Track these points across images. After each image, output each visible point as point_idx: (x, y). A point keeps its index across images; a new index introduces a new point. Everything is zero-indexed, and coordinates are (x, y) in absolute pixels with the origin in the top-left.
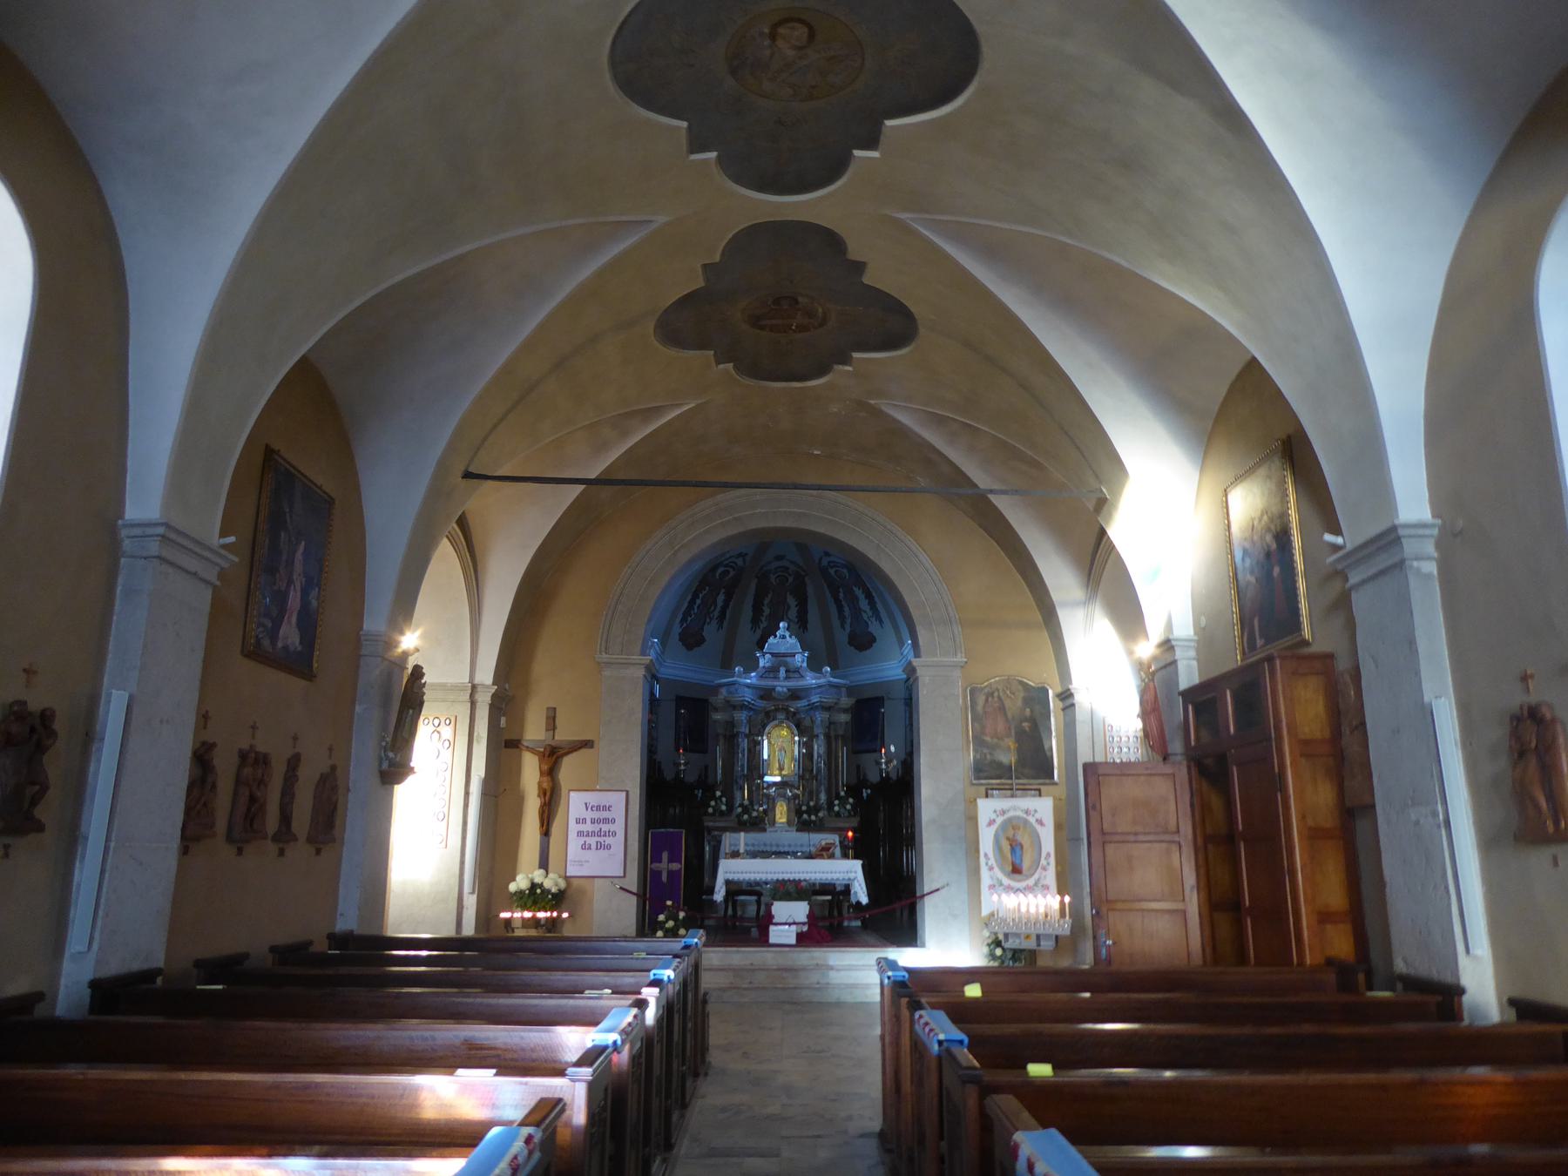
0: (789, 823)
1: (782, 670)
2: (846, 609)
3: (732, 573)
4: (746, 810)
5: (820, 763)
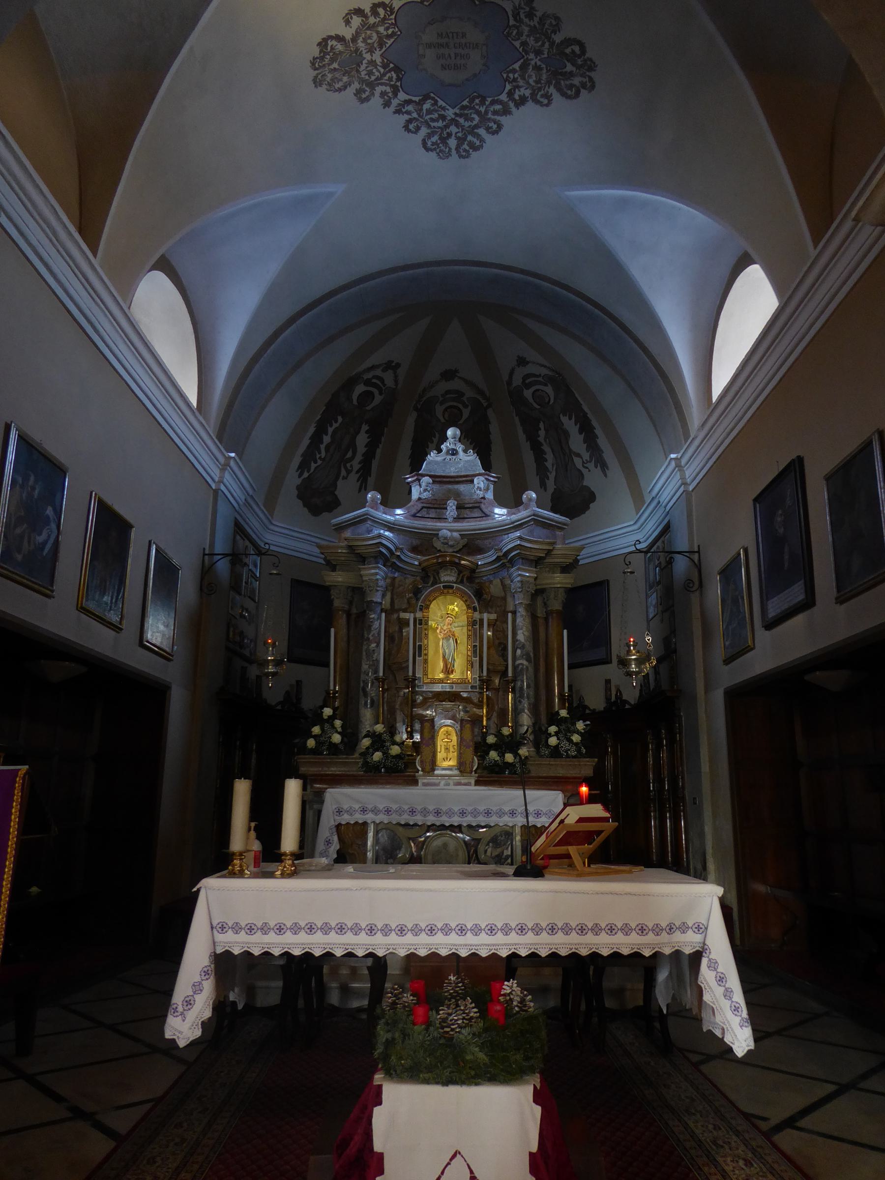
0: (462, 767)
1: (452, 505)
2: (550, 457)
3: (378, 399)
4: (378, 742)
5: (517, 658)
